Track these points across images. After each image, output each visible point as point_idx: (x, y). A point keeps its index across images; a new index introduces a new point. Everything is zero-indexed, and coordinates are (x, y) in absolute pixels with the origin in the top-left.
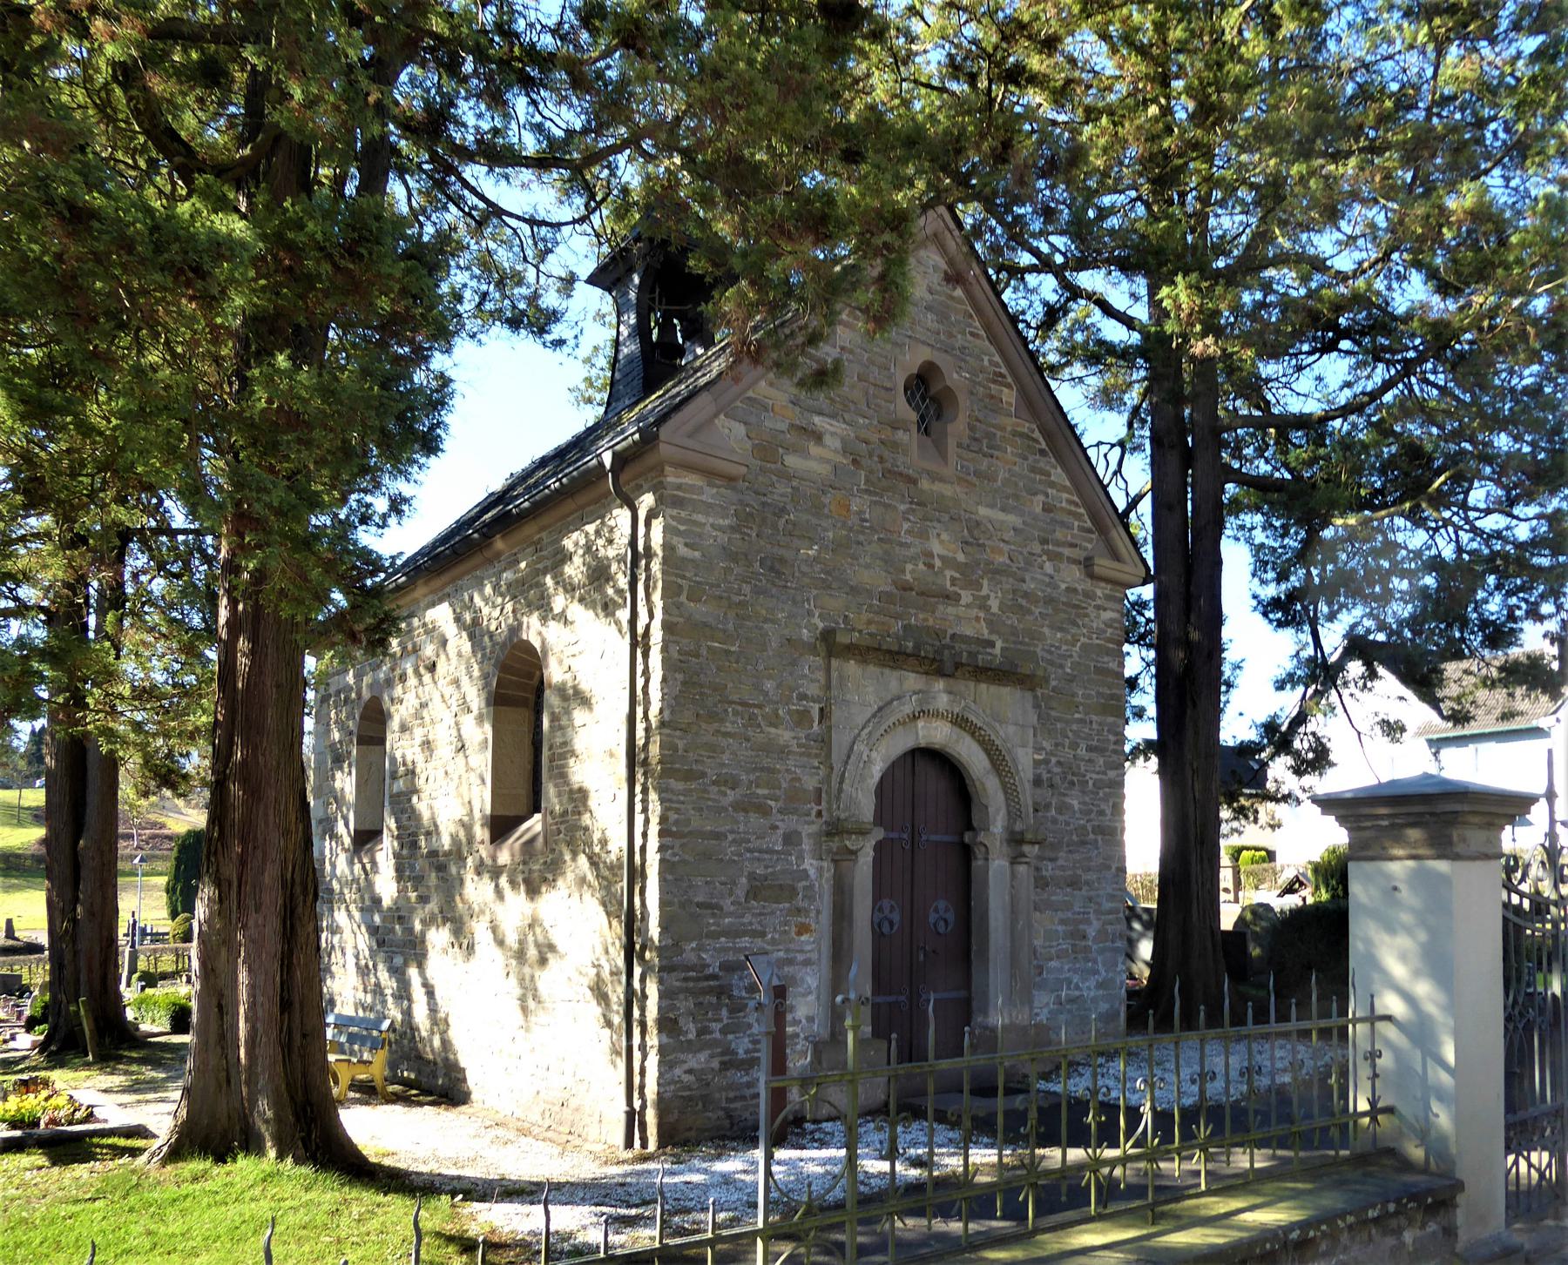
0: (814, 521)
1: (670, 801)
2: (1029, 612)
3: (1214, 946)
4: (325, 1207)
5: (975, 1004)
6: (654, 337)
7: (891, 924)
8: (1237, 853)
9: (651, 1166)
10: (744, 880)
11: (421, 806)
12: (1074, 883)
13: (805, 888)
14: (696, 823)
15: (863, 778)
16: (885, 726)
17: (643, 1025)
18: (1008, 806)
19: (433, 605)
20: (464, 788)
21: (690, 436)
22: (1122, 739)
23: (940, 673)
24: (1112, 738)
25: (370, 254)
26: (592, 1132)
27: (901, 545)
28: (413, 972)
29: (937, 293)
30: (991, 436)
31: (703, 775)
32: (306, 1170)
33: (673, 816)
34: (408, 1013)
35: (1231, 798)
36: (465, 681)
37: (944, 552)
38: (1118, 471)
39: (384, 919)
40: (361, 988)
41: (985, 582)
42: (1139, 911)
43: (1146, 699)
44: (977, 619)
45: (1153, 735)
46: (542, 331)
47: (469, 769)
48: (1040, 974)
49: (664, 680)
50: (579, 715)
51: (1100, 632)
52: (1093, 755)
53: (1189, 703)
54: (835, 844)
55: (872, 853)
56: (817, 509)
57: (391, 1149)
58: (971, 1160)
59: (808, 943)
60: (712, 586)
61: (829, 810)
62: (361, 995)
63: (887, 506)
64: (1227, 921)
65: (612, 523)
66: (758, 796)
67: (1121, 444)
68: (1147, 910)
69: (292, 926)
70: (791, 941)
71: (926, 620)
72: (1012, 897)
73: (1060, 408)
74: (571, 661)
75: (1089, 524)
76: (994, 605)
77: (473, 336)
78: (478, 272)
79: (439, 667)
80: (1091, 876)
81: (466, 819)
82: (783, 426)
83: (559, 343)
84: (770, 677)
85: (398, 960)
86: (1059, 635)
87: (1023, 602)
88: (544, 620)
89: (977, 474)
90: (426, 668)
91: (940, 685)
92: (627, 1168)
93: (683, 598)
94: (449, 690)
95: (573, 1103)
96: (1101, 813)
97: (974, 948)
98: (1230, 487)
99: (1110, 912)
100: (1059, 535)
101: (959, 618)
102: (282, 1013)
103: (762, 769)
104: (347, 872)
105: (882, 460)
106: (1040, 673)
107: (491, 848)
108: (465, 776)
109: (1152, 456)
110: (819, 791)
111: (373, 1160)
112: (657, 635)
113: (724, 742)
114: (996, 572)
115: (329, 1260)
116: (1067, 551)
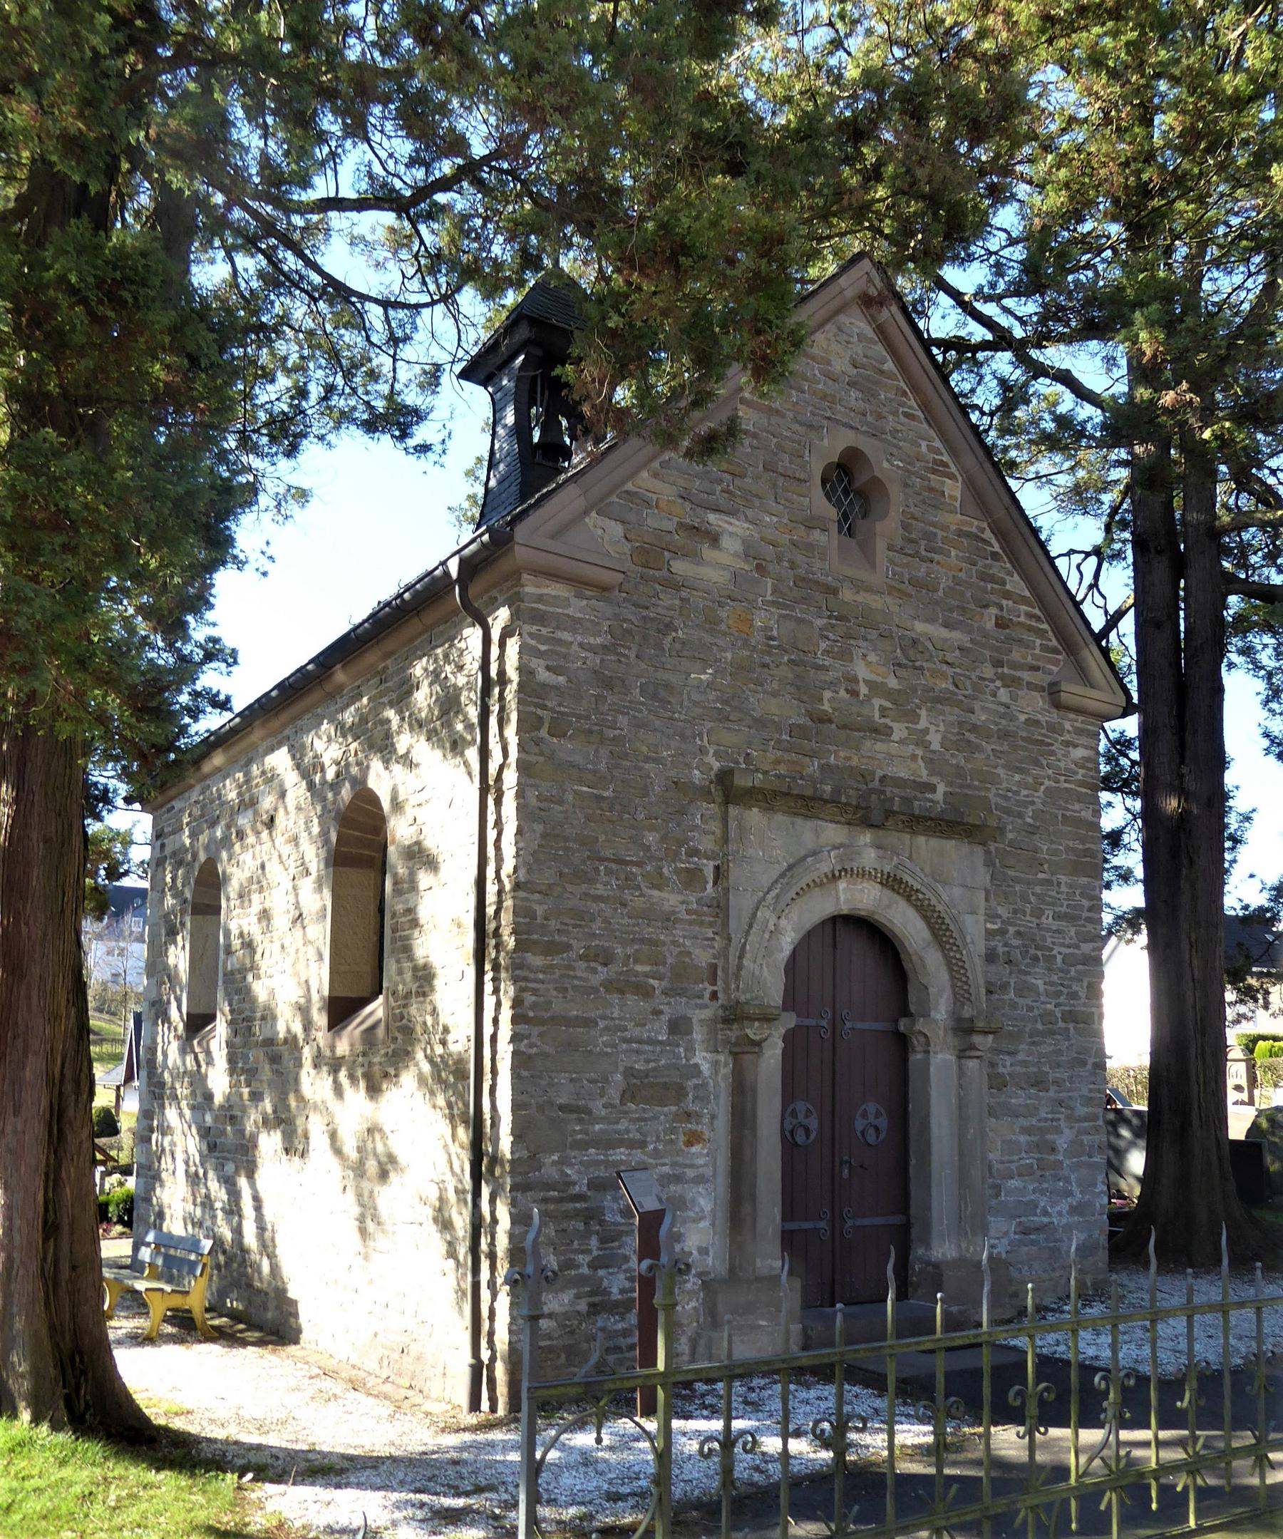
0: (708, 639)
1: (526, 979)
2: (979, 749)
3: (1220, 1159)
4: (77, 1489)
5: (914, 1232)
6: (536, 440)
7: (807, 1132)
8: (1251, 1044)
9: (497, 1435)
10: (619, 1077)
11: (260, 990)
12: (1038, 1083)
13: (696, 1087)
14: (558, 1007)
15: (769, 952)
16: (796, 889)
17: (492, 1256)
18: (954, 986)
19: (272, 750)
20: (301, 966)
21: (553, 537)
22: (1098, 906)
23: (867, 822)
24: (1086, 903)
25: (135, 299)
26: (435, 1388)
27: (819, 668)
28: (243, 1182)
29: (863, 367)
30: (930, 537)
31: (568, 947)
32: (64, 1438)
33: (529, 998)
34: (238, 1231)
35: (1236, 977)
36: (304, 838)
37: (872, 677)
38: (1094, 586)
39: (216, 1119)
40: (190, 1199)
41: (923, 713)
42: (1128, 1114)
43: (1132, 858)
44: (914, 757)
45: (1141, 902)
46: (404, 435)
47: (306, 942)
48: (998, 1195)
49: (519, 832)
50: (424, 879)
51: (1069, 774)
52: (1063, 924)
53: (1185, 861)
54: (733, 1033)
55: (781, 1044)
56: (712, 623)
57: (187, 1406)
58: (899, 1439)
59: (700, 1155)
60: (579, 717)
61: (726, 990)
62: (190, 1207)
63: (800, 621)
64: (1238, 1125)
65: (462, 645)
66: (637, 974)
67: (1097, 552)
68: (1138, 1113)
69: (60, 1131)
70: (679, 1153)
71: (848, 758)
72: (960, 1098)
73: (1021, 510)
74: (417, 812)
75: (1054, 643)
76: (935, 740)
77: (321, 438)
78: (323, 362)
79: (277, 821)
80: (1062, 1074)
81: (302, 1001)
82: (671, 526)
83: (424, 449)
84: (652, 829)
85: (230, 1168)
86: (1017, 777)
87: (972, 737)
88: (386, 762)
89: (914, 582)
90: (263, 823)
91: (866, 837)
92: (467, 1437)
93: (543, 733)
94: (286, 849)
95: (415, 1349)
96: (1074, 996)
97: (913, 1162)
98: (1233, 599)
99: (1086, 1119)
100: (1016, 655)
101: (891, 757)
102: (46, 1240)
103: (642, 941)
104: (179, 1063)
105: (793, 565)
106: (993, 823)
107: (329, 1035)
108: (302, 949)
109: (1134, 564)
110: (714, 968)
111: (161, 1421)
112: (511, 778)
113: (594, 907)
114: (937, 700)
115: (126, 1533)
116: (1026, 676)
